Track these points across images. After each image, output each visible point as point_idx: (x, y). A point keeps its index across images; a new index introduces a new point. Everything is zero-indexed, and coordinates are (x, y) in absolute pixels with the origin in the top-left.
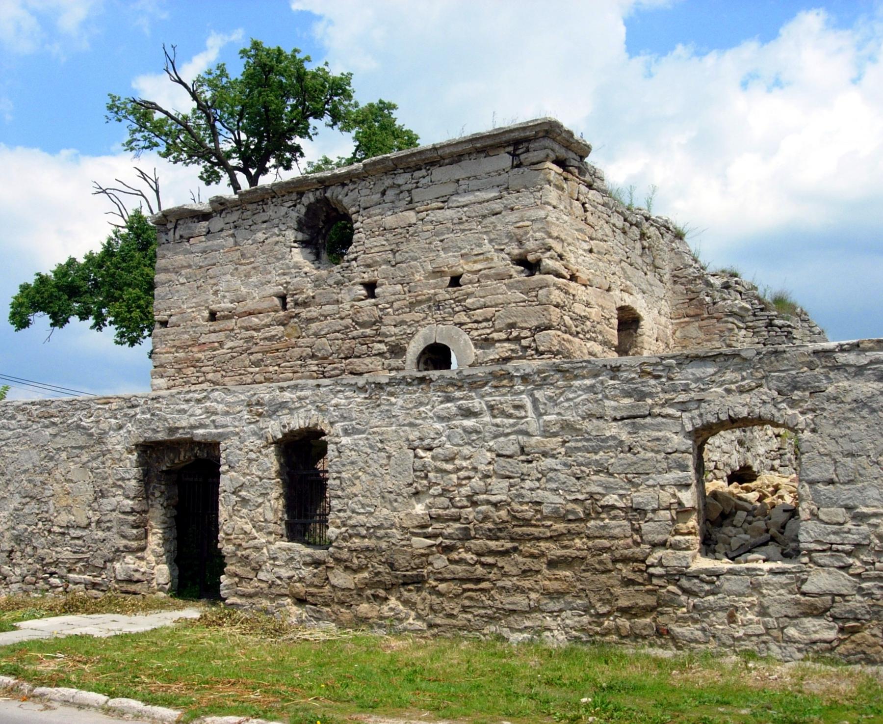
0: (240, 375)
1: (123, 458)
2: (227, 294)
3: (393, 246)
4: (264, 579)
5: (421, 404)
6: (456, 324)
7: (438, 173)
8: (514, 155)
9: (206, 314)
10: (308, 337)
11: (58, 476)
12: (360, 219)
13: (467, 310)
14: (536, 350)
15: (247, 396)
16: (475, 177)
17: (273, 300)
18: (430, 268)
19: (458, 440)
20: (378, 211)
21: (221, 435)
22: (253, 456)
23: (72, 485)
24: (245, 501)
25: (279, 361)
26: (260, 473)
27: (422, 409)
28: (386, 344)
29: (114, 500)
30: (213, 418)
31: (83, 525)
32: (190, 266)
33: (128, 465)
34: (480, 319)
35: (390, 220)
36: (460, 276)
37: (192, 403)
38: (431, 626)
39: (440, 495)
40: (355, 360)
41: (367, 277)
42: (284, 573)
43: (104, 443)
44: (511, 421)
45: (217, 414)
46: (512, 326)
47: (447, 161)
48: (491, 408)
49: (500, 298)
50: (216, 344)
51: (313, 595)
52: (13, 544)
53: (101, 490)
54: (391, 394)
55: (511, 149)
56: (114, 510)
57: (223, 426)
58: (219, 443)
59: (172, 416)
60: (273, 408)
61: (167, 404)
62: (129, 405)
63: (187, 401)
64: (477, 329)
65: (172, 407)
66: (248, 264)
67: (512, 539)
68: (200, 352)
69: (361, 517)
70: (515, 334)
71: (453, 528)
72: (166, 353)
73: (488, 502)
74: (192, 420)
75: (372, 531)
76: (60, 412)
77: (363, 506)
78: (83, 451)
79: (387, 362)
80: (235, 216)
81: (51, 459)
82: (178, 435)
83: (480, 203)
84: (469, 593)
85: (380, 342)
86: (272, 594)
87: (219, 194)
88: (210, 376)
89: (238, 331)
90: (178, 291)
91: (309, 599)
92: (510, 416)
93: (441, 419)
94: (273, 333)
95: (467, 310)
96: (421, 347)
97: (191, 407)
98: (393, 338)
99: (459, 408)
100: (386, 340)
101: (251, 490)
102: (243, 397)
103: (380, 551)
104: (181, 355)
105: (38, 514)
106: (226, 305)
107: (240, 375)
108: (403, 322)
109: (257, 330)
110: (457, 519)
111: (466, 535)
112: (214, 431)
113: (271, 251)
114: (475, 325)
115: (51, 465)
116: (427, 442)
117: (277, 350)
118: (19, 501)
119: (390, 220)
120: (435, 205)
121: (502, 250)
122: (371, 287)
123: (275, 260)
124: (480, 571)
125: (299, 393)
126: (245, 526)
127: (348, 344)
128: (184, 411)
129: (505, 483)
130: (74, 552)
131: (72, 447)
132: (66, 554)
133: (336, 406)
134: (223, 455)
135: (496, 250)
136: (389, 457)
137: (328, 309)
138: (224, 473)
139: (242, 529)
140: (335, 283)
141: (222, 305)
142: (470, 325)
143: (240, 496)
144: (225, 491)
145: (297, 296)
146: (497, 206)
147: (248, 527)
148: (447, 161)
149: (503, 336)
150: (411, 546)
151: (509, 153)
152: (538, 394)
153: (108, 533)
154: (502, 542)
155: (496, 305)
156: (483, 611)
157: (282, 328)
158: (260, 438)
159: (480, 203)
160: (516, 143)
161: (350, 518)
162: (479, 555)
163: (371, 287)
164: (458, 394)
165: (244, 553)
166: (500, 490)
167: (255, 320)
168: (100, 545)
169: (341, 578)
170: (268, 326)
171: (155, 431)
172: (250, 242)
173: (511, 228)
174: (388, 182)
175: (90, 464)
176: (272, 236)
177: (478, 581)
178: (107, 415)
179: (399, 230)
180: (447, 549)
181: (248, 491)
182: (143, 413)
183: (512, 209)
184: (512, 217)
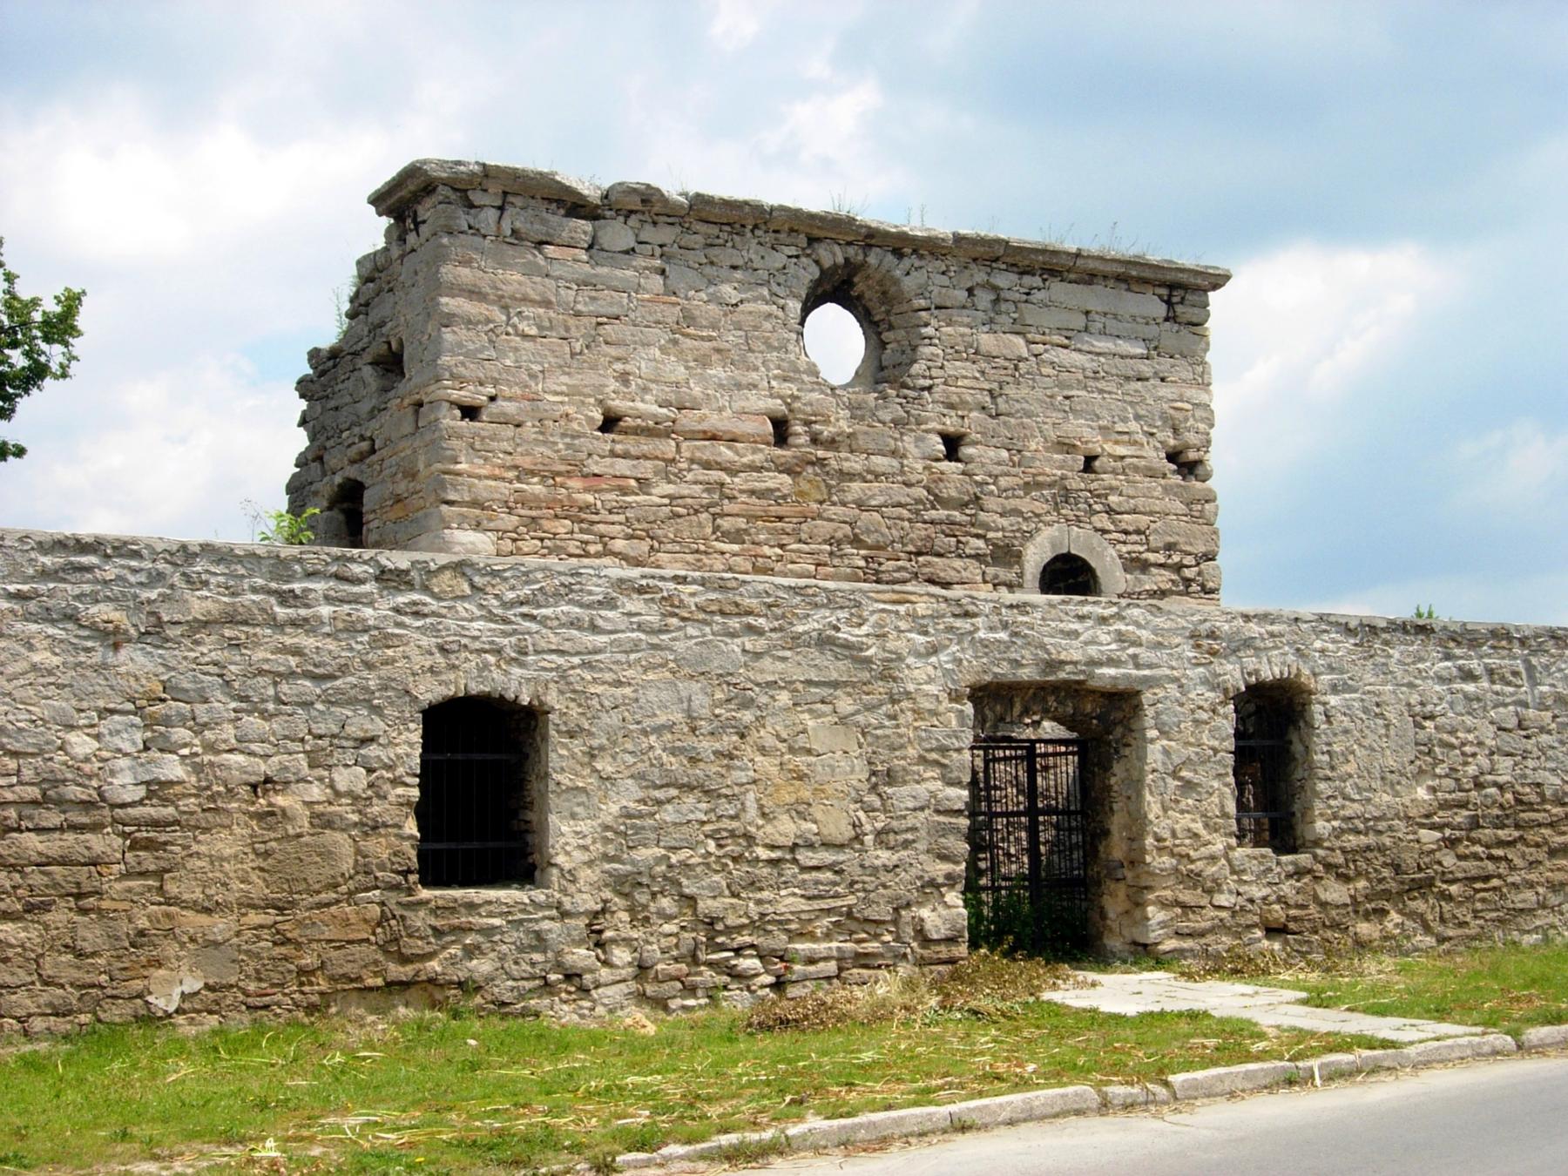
0: (697, 551)
1: (941, 709)
2: (653, 386)
3: (995, 386)
4: (1226, 904)
5: (1422, 660)
6: (1096, 530)
7: (1058, 289)
8: (1169, 303)
9: (598, 417)
10: (844, 504)
11: (770, 741)
12: (933, 322)
13: (1110, 511)
14: (1203, 586)
15: (1192, 623)
16: (1115, 316)
17: (764, 423)
18: (1053, 436)
19: (1460, 708)
20: (966, 320)
21: (1146, 679)
22: (1204, 716)
23: (814, 759)
24: (1188, 786)
25: (785, 540)
26: (1216, 743)
27: (1420, 666)
28: (986, 540)
29: (921, 790)
30: (1131, 651)
31: (840, 840)
32: (547, 304)
33: (954, 723)
34: (1131, 529)
35: (986, 341)
36: (1096, 457)
37: (1089, 623)
38: (1442, 940)
39: (1447, 776)
40: (936, 559)
41: (951, 424)
42: (1257, 892)
43: (895, 679)
44: (1511, 689)
45: (1141, 645)
46: (1170, 547)
47: (1072, 276)
48: (1491, 672)
49: (1158, 506)
50: (633, 483)
51: (1295, 919)
52: (607, 894)
53: (889, 770)
54: (1386, 643)
55: (1164, 292)
56: (922, 809)
57: (1150, 666)
58: (1138, 693)
59: (1052, 641)
60: (1233, 645)
61: (1043, 619)
62: (958, 611)
63: (1081, 618)
64: (1124, 543)
65: (1053, 624)
66: (702, 338)
67: (1517, 826)
68: (587, 490)
69: (1356, 805)
70: (1176, 558)
71: (1461, 817)
72: (487, 478)
73: (1495, 784)
74: (1093, 651)
75: (1370, 825)
76: (770, 606)
77: (1359, 790)
78: (839, 692)
79: (991, 571)
80: (666, 234)
81: (747, 704)
82: (1062, 675)
83: (1122, 357)
84: (1482, 894)
85: (978, 536)
86: (1239, 925)
87: (654, 184)
88: (619, 545)
89: (684, 465)
90: (516, 350)
91: (1292, 925)
92: (1509, 684)
93: (1441, 679)
94: (770, 484)
95: (1110, 511)
96: (1048, 556)
97: (1087, 629)
98: (1000, 534)
99: (1460, 669)
100: (990, 535)
101: (1200, 769)
102: (1183, 623)
103: (1381, 849)
104: (535, 488)
105: (703, 823)
106: (649, 406)
107: (697, 551)
108: (1017, 512)
109: (733, 472)
110: (1463, 805)
111: (1475, 824)
112: (1134, 672)
113: (756, 328)
114: (1122, 537)
115: (747, 716)
116: (1429, 708)
117: (775, 515)
118: (641, 794)
119: (986, 341)
120: (1057, 339)
121: (1152, 434)
122: (953, 445)
123: (763, 347)
124: (1490, 866)
125: (1270, 628)
126: (1193, 825)
127: (920, 531)
128: (1075, 634)
129: (1509, 762)
130: (809, 898)
131: (809, 682)
132: (789, 902)
133: (1322, 651)
134: (1150, 712)
135: (1145, 433)
136: (1387, 726)
137: (880, 462)
138: (1152, 741)
139: (1189, 830)
140: (893, 421)
141: (640, 405)
142: (1115, 536)
143: (1181, 779)
144: (1154, 771)
145: (817, 427)
146: (1145, 368)
147: (1198, 827)
148: (1072, 276)
149: (1160, 558)
150: (1418, 841)
151: (1160, 297)
152: (1534, 661)
153: (904, 853)
154: (1506, 831)
155: (1151, 513)
156: (1495, 914)
157: (786, 479)
158: (1213, 689)
159: (1122, 357)
160: (1172, 286)
161: (1343, 807)
162: (1488, 847)
163: (953, 445)
164: (1458, 652)
165: (1192, 867)
166: (1505, 770)
167: (725, 453)
168: (885, 877)
169: (1335, 892)
170: (759, 469)
171: (1017, 664)
172: (703, 295)
173: (1165, 406)
174: (980, 276)
175: (860, 718)
176: (755, 300)
177: (1487, 879)
178: (903, 625)
179: (1001, 362)
180: (1451, 843)
181: (1196, 772)
182: (991, 629)
183: (1163, 380)
184: (1165, 391)
